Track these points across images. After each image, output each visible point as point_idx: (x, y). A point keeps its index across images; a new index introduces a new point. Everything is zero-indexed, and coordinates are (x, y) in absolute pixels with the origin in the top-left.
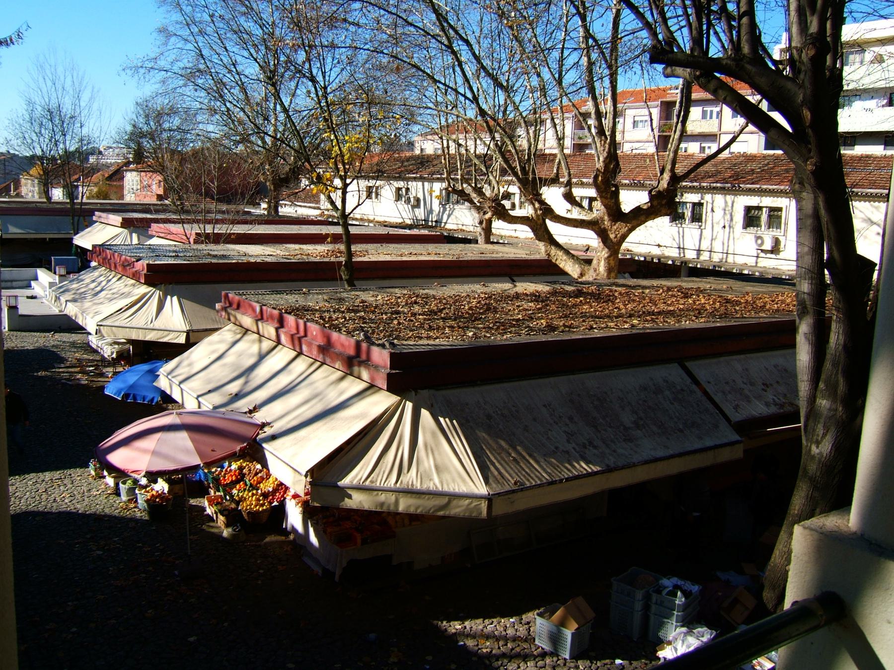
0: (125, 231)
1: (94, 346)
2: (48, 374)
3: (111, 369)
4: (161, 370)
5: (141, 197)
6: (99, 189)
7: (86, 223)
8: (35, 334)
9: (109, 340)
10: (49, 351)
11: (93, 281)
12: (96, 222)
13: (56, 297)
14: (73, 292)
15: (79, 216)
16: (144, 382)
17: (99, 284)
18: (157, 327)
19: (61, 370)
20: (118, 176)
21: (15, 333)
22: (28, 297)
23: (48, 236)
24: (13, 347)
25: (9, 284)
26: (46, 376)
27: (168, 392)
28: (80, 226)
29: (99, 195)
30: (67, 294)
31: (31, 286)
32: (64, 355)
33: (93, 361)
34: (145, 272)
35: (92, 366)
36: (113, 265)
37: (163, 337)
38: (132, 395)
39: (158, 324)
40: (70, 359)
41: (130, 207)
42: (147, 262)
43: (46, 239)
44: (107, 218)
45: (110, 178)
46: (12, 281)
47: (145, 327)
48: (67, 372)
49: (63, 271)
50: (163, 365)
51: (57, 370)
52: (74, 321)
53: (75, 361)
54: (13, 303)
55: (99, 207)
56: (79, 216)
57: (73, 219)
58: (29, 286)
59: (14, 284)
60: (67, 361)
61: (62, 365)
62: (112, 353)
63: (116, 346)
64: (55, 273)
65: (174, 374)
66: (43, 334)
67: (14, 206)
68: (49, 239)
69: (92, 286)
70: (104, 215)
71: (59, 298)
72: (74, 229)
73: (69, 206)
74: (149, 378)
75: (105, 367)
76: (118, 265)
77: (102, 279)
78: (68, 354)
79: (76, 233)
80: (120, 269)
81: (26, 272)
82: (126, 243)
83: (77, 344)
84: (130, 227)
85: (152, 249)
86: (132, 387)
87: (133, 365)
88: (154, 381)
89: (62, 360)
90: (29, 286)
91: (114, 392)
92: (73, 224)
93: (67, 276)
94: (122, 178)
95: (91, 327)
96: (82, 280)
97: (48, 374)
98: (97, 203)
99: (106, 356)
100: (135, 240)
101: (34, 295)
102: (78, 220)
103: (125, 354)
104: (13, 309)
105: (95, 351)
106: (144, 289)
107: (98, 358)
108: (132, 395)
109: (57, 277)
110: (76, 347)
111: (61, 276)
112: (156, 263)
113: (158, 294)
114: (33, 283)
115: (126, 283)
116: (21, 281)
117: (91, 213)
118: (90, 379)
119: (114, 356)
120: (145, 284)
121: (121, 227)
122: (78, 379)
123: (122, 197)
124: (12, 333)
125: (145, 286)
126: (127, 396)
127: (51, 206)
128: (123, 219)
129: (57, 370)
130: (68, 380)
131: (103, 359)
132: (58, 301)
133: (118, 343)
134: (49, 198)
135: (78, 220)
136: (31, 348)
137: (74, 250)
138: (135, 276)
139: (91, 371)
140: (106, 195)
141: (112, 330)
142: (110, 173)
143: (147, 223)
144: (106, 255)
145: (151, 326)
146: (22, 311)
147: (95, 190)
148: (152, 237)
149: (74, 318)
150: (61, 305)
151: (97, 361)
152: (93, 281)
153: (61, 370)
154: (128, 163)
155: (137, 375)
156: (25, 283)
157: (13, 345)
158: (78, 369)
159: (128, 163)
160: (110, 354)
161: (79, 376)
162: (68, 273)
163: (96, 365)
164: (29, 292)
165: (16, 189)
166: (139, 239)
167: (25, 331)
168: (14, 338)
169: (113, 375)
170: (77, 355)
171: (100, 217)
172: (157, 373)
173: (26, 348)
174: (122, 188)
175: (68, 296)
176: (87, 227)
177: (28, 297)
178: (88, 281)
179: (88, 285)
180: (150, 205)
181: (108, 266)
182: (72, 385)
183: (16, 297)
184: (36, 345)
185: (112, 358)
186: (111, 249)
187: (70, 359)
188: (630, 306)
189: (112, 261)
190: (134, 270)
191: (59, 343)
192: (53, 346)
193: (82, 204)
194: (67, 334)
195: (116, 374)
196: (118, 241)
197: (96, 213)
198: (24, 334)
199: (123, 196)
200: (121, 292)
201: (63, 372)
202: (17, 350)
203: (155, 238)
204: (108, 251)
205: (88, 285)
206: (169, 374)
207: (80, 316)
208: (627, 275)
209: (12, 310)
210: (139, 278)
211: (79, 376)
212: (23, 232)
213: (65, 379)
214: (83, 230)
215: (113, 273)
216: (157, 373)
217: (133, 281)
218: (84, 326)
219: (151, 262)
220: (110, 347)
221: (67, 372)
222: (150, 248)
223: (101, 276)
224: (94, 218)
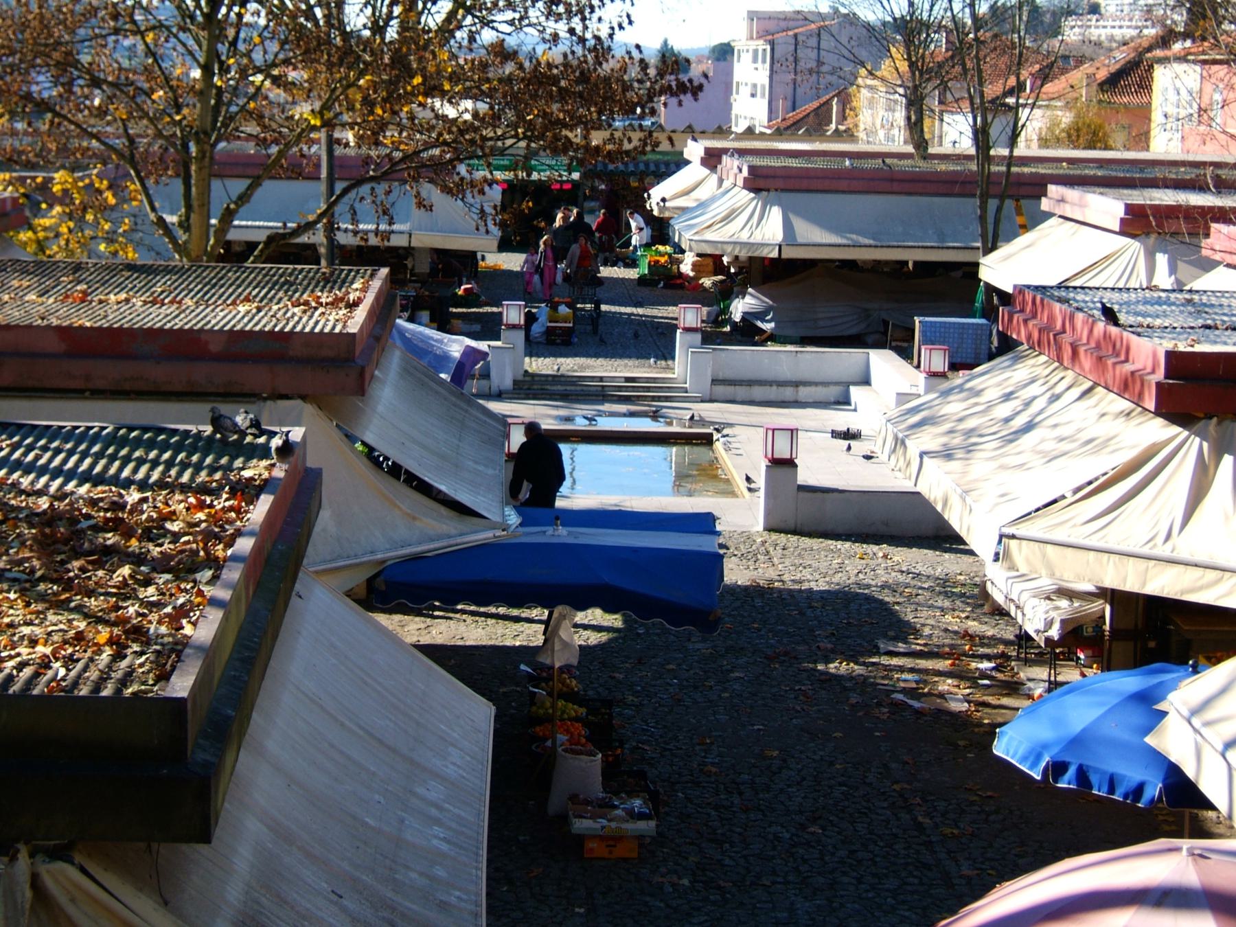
0: (1134, 247)
1: (999, 598)
2: (858, 669)
3: (1041, 673)
4: (1172, 696)
5: (1194, 143)
6: (1078, 116)
7: (1020, 220)
8: (839, 544)
9: (1046, 583)
10: (869, 599)
11: (1008, 397)
12: (1049, 215)
13: (896, 438)
14: (947, 426)
15: (1002, 198)
16: (1117, 729)
17: (1027, 404)
18: (1182, 554)
19: (895, 661)
20: (1134, 78)
21: (782, 539)
22: (836, 434)
23: (911, 257)
24: (772, 581)
25: (788, 393)
26: (850, 677)
27: (1190, 772)
28: (1003, 226)
29: (1074, 136)
30: (930, 430)
31: (848, 403)
32: (910, 617)
33: (994, 641)
34: (1160, 375)
35: (989, 658)
36: (1067, 352)
37: (1201, 588)
38: (1072, 771)
39: (1184, 546)
40: (927, 631)
41: (1158, 173)
42: (1168, 345)
43: (906, 263)
44: (1082, 205)
45: (1113, 82)
46: (797, 384)
47: (1146, 551)
48: (912, 670)
49: (937, 360)
50: (1180, 679)
51: (885, 660)
52: (939, 517)
53: (939, 639)
54: (783, 452)
55: (1064, 169)
56: (1002, 198)
57: (983, 207)
58: (843, 401)
59: (804, 393)
60: (916, 632)
61: (901, 647)
62: (1049, 624)
63: (1064, 603)
64: (918, 367)
65: (1210, 714)
66: (859, 548)
67: (820, 164)
68: (916, 263)
69: (1004, 410)
70: (1072, 194)
71: (903, 443)
72: (984, 237)
73: (974, 167)
74: (1136, 716)
75: (1028, 662)
76: (1082, 350)
77: (1034, 390)
78: (925, 613)
79: (989, 249)
80: (1087, 362)
81: (843, 359)
82: (1132, 284)
83: (955, 584)
84: (1147, 234)
85: (1195, 304)
86: (1077, 742)
87: (1109, 670)
88: (1148, 730)
89: (904, 630)
90: (843, 401)
91: (1021, 752)
92: (982, 219)
93: (950, 374)
94: (1145, 85)
95: (981, 540)
96: (978, 393)
97: (858, 669)
98: (1060, 160)
99: (1030, 629)
100: (1164, 279)
101: (854, 427)
102: (999, 210)
103: (1089, 631)
104: (782, 465)
105: (1000, 612)
106: (1160, 430)
107: (1009, 634)
108: (1072, 771)
109: (920, 378)
110: (947, 595)
111: (933, 375)
112: (1198, 348)
113: (1195, 446)
114: (856, 392)
115: (1102, 408)
116: (769, 383)
117: (1037, 187)
118: (978, 697)
119: (1054, 632)
120: (1158, 413)
121: (1122, 233)
122: (941, 696)
123: (1143, 139)
124: (774, 536)
125: (1160, 421)
126: (1058, 768)
127: (923, 166)
128: (1129, 208)
129: (885, 660)
130: (912, 693)
131: (1024, 639)
132: (900, 451)
133: (1070, 594)
134: (921, 143)
135: (999, 210)
136: (821, 586)
137: (980, 296)
138: (1128, 387)
139: (984, 675)
140: (1095, 134)
141: (1044, 555)
142: (1113, 69)
143: (1201, 220)
144: (1051, 318)
145: (1164, 551)
146: (807, 474)
147: (1066, 118)
148: (1208, 265)
149: (939, 508)
150: (909, 464)
151: (1007, 643)
152: (1008, 397)
153: (895, 661)
154: (1165, 40)
155: (1102, 704)
156: (833, 392)
157: (772, 574)
158: (944, 664)
159: (1165, 40)
160: (1041, 626)
161: (946, 685)
162: (955, 367)
163: (1003, 655)
164: (840, 419)
165: (843, 118)
166: (1173, 270)
167: (810, 535)
168: (776, 554)
169: (1049, 690)
170: (948, 618)
171: (1062, 200)
172: (1161, 706)
173: (805, 586)
174: (1145, 113)
175: (929, 439)
176: (1025, 228)
177: (836, 434)
178: (992, 394)
179: (990, 407)
180: (1203, 164)
181: (1053, 353)
182: (919, 713)
183: (793, 432)
184: (836, 579)
185: (1048, 641)
186: (1065, 301)
187: (927, 631)
188: (63, 129)
189: (1066, 339)
190: (1128, 367)
191: (901, 578)
192: (884, 586)
193: (1011, 160)
194: (929, 553)
195: (1053, 686)
196: (1107, 278)
197: (1052, 189)
198: (807, 542)
199: (1147, 134)
200: (1085, 436)
201: (901, 669)
202: (780, 591)
203: (1221, 268)
204: (1057, 306)
205: (990, 407)
206: (1195, 712)
207: (955, 501)
208: (425, 315)
209: (782, 471)
210: (1141, 395)
211: (946, 685)
212: (844, 241)
213: (904, 691)
214: (1010, 238)
215: (1070, 375)
216: (1161, 706)
217: (1126, 405)
218: (963, 534)
219: (1182, 347)
220: (1046, 605)
221: (912, 670)
222: (1189, 301)
223: (1033, 381)
224: (1045, 204)
